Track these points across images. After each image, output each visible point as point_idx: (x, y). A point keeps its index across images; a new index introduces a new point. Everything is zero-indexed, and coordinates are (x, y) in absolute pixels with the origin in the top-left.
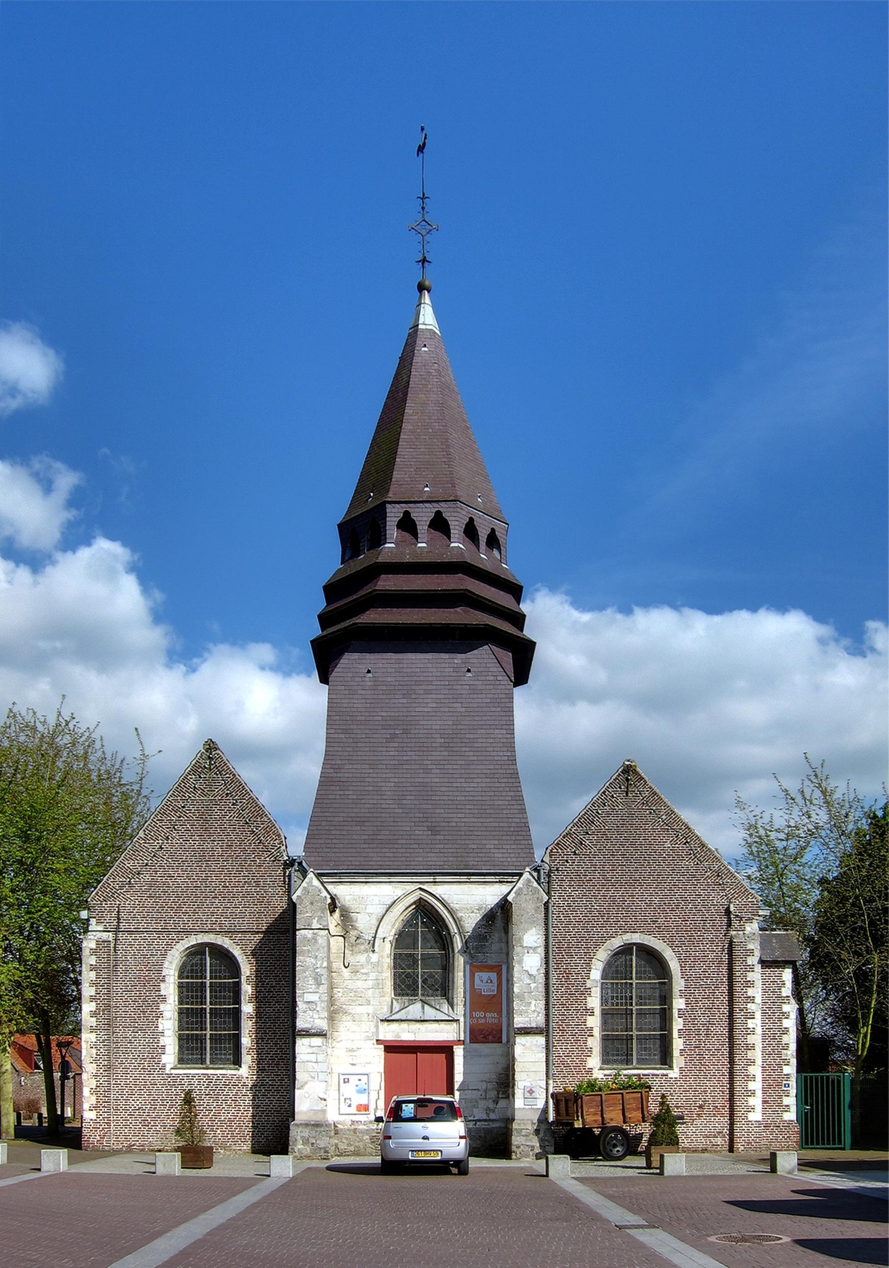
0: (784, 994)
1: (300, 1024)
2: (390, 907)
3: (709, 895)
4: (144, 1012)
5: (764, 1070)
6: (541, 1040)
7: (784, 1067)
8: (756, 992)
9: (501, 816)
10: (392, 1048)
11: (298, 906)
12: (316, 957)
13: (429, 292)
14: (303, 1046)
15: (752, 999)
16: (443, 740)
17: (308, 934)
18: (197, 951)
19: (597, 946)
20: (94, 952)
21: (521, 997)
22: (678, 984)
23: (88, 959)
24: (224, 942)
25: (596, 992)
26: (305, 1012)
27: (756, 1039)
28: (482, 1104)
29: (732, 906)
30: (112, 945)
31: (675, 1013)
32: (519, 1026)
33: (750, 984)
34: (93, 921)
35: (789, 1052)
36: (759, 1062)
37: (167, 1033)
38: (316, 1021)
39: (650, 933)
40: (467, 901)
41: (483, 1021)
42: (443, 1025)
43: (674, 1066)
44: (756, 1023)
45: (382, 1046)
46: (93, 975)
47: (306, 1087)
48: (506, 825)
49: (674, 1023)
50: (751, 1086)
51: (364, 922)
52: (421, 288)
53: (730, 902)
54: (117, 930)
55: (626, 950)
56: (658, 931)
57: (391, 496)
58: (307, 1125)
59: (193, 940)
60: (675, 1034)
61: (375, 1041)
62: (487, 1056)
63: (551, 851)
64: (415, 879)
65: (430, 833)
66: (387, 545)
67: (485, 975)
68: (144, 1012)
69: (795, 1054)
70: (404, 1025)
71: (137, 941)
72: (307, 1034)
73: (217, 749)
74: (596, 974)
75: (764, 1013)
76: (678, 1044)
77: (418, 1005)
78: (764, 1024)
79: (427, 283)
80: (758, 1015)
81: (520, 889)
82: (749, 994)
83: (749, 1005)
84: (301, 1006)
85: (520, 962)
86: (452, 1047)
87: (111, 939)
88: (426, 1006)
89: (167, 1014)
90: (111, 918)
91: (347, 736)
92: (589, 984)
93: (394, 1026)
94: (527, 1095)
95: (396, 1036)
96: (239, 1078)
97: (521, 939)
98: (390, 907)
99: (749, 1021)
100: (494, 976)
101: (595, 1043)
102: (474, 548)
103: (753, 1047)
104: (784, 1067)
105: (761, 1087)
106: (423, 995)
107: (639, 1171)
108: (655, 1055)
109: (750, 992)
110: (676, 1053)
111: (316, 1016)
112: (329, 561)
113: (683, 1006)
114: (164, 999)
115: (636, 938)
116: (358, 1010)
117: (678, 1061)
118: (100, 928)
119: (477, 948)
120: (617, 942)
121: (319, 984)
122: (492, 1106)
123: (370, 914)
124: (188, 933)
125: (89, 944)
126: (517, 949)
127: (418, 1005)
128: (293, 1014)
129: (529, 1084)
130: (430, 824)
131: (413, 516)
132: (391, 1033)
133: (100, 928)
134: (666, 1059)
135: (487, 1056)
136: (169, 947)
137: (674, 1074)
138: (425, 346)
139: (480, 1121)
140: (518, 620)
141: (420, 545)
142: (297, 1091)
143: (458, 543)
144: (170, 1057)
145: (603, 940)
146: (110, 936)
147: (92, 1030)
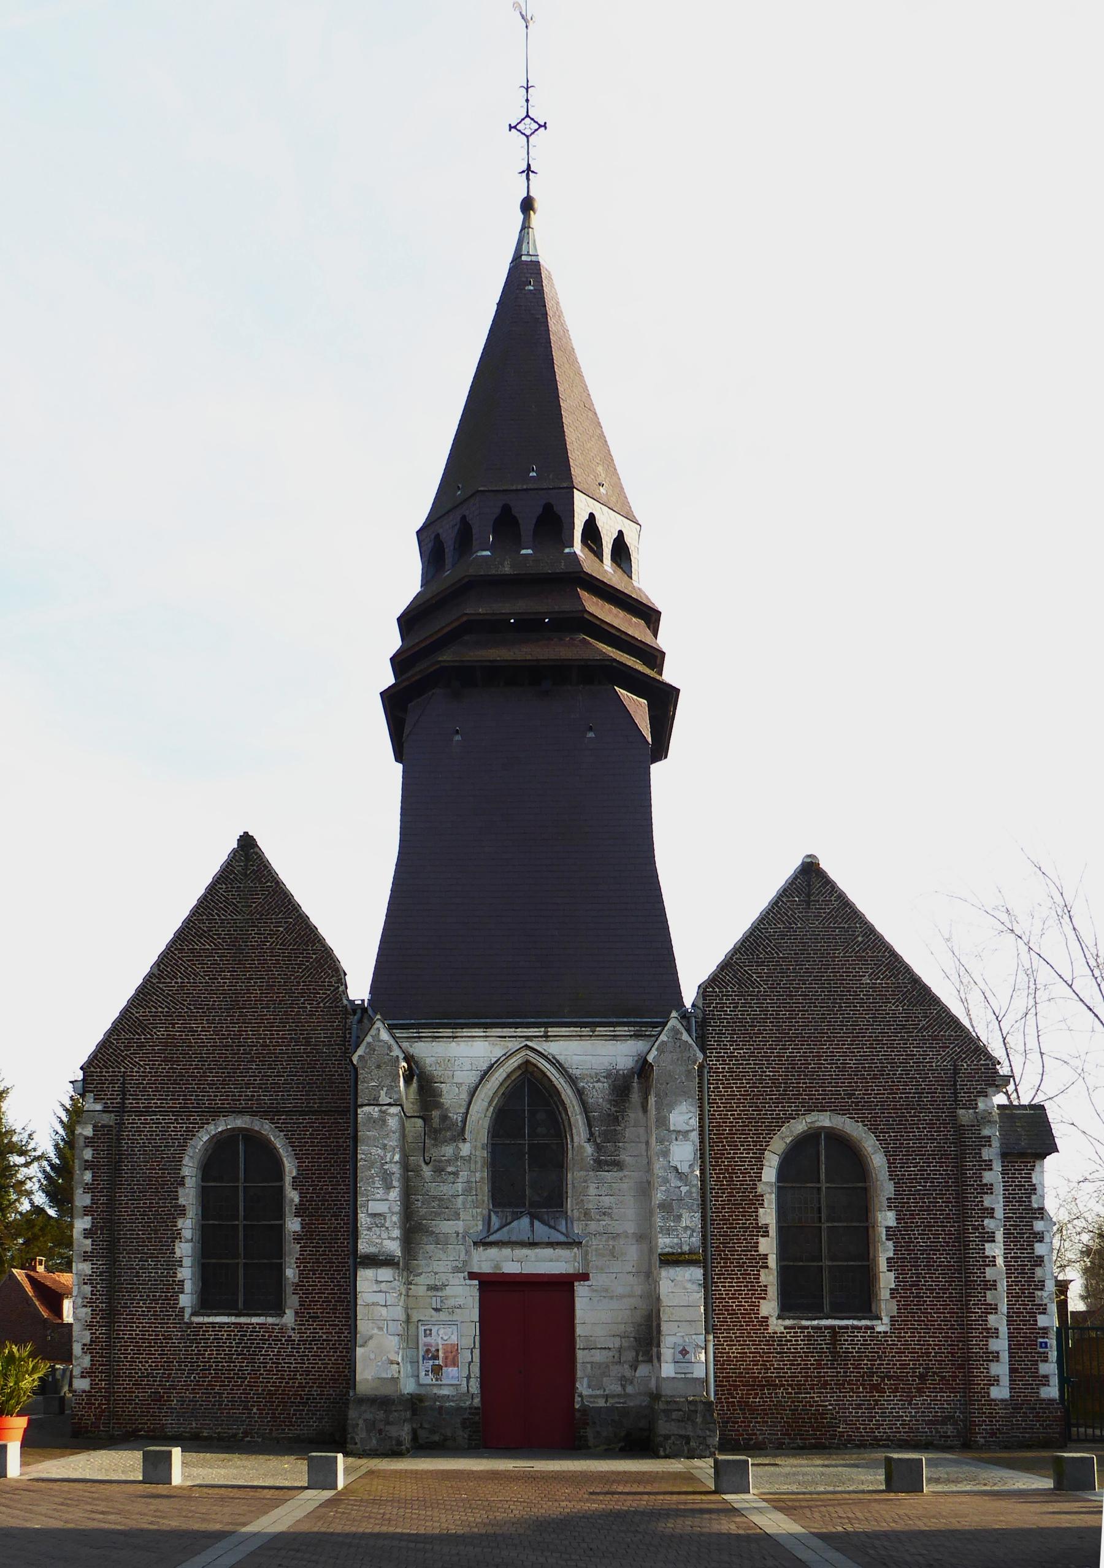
1: (363, 1247)
2: (486, 1073)
4: (156, 1231)
5: (1010, 1322)
6: (697, 1273)
8: (996, 1202)
10: (492, 1286)
17: (374, 1111)
18: (222, 1145)
22: (886, 1188)
24: (265, 1128)
28: (615, 1370)
44: (996, 1250)
45: (477, 1282)
47: (371, 1343)
50: (995, 1345)
51: (452, 1096)
54: (121, 1110)
59: (221, 1125)
62: (621, 1297)
68: (156, 1231)
70: (507, 1251)
74: (769, 1174)
75: (1007, 1234)
76: (886, 1280)
77: (525, 1221)
78: (1007, 1249)
80: (999, 1236)
82: (986, 1204)
88: (536, 1223)
89: (187, 1234)
93: (493, 1252)
96: (283, 1329)
99: (987, 1245)
101: (769, 1278)
103: (993, 1286)
104: (1039, 1317)
109: (988, 1201)
113: (892, 1223)
114: (182, 1211)
115: (825, 1120)
117: (887, 1307)
120: (799, 1126)
121: (389, 1187)
122: (628, 1373)
124: (216, 1113)
127: (525, 1221)
128: (354, 1234)
129: (680, 1341)
132: (487, 1261)
134: (863, 1303)
139: (613, 1396)
140: (655, 658)
141: (523, 552)
144: (186, 1300)
145: (780, 1122)
147: (86, 1257)
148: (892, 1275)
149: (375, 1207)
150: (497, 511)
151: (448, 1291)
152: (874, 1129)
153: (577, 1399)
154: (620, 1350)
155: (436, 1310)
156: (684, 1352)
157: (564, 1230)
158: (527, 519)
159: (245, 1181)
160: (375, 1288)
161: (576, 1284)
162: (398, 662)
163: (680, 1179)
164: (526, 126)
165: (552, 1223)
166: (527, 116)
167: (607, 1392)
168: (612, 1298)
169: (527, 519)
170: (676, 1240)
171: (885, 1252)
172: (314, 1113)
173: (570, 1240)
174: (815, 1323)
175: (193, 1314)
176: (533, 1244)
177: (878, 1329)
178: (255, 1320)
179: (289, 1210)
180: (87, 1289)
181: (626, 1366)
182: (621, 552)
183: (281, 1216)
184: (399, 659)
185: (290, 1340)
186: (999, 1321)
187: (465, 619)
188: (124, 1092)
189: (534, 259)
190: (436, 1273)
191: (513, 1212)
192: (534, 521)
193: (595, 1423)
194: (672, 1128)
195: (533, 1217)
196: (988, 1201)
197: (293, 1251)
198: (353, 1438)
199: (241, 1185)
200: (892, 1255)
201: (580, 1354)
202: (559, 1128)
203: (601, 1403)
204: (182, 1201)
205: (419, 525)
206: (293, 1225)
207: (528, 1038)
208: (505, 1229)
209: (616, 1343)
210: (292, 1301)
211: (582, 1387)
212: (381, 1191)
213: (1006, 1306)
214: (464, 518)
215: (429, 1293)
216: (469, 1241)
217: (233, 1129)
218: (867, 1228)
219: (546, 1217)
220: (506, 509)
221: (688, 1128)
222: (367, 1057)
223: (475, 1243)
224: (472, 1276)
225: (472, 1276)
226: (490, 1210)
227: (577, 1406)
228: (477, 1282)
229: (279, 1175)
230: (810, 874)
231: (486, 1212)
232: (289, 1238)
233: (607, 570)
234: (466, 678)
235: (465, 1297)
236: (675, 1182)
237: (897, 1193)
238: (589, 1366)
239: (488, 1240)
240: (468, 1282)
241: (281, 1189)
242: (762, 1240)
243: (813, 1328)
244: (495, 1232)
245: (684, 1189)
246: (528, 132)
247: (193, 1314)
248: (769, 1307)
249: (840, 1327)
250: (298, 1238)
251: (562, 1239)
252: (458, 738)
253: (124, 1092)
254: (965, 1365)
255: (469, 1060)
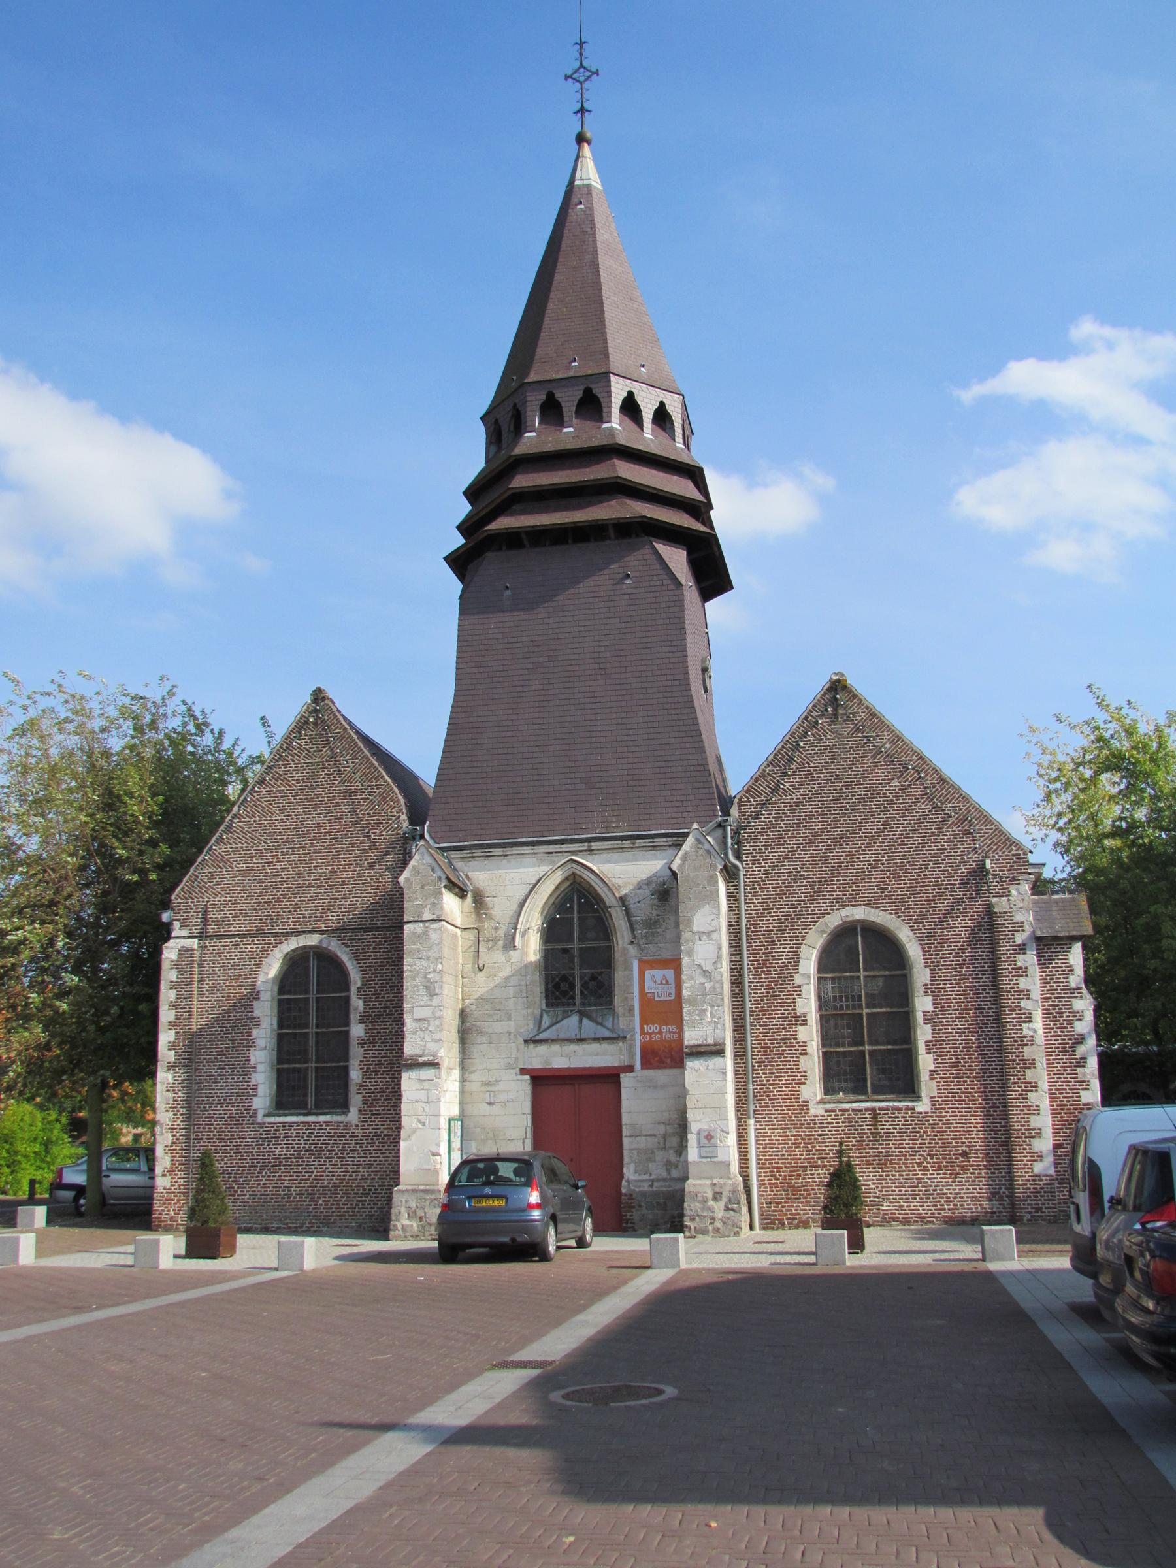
0: (1073, 985)
1: (410, 1048)
2: (535, 886)
3: (955, 849)
4: (233, 1041)
5: (1052, 1097)
7: (1082, 1093)
9: (673, 758)
10: (541, 1080)
11: (406, 892)
12: (428, 959)
13: (589, 144)
14: (409, 1081)
15: (1026, 994)
16: (597, 666)
19: (806, 927)
20: (176, 964)
21: (693, 1003)
22: (921, 976)
23: (169, 975)
25: (810, 991)
26: (415, 1033)
27: (1037, 1053)
28: (660, 1156)
29: (988, 862)
30: (197, 955)
31: (919, 1017)
32: (693, 1042)
33: (1021, 972)
34: (177, 924)
35: (1088, 1071)
36: (1044, 1085)
37: (260, 1068)
38: (429, 1045)
39: (876, 905)
40: (623, 872)
41: (657, 1037)
42: (605, 1046)
43: (923, 1094)
45: (528, 1077)
46: (172, 994)
47: (414, 1138)
48: (680, 769)
49: (919, 1032)
50: (1035, 1122)
52: (581, 139)
53: (987, 857)
55: (847, 931)
56: (889, 903)
57: (532, 377)
58: (414, 1191)
59: (293, 944)
60: (921, 1047)
61: (518, 1071)
62: (664, 1087)
63: (740, 800)
64: (565, 847)
65: (583, 786)
66: (527, 435)
67: (658, 973)
68: (233, 1041)
69: (1096, 1073)
70: (556, 1048)
71: (226, 948)
72: (416, 1065)
73: (324, 699)
75: (1046, 1013)
76: (926, 1062)
77: (575, 1018)
78: (1047, 1029)
79: (588, 135)
80: (1038, 1017)
81: (687, 853)
82: (1022, 986)
83: (1023, 1003)
84: (409, 1025)
85: (690, 953)
86: (618, 1076)
87: (196, 947)
88: (585, 1020)
89: (261, 1043)
90: (195, 919)
91: (481, 670)
92: (798, 980)
93: (543, 1048)
94: (704, 1141)
95: (547, 1062)
96: (347, 1126)
97: (689, 922)
98: (535, 886)
99: (1025, 1025)
100: (670, 973)
101: (812, 1063)
102: (633, 426)
103: (1033, 1065)
104: (1082, 1093)
105: (1050, 1123)
106: (583, 1004)
107: (937, 1256)
108: (898, 1079)
109: (1023, 983)
110: (924, 1075)
111: (428, 1038)
112: (471, 458)
113: (930, 1008)
114: (257, 1022)
115: (859, 913)
116: (498, 1027)
117: (928, 1087)
118: (185, 933)
119: (647, 936)
120: (834, 920)
123: (509, 898)
125: (170, 953)
126: (686, 936)
127: (575, 1018)
128: (399, 1037)
129: (705, 1127)
130: (583, 775)
131: (638, 398)
133: (185, 933)
134: (908, 1087)
135: (664, 1087)
136: (265, 953)
137: (923, 1106)
138: (581, 203)
139: (658, 1180)
141: (566, 430)
142: (403, 1144)
143: (615, 422)
144: (261, 1102)
145: (815, 917)
146: (194, 943)
147: (170, 1067)
148: (931, 1057)
149: (419, 1013)
150: (543, 397)
151: (501, 1086)
152: (907, 918)
153: (624, 1183)
154: (665, 1137)
155: (490, 1104)
156: (709, 1137)
157: (610, 1025)
158: (569, 399)
159: (318, 992)
160: (418, 1086)
161: (622, 1075)
162: (466, 528)
163: (704, 976)
164: (582, 75)
165: (600, 1019)
166: (581, 66)
167: (653, 1177)
168: (655, 1087)
169: (569, 399)
170: (701, 1033)
171: (923, 1034)
172: (377, 929)
173: (615, 1035)
174: (855, 1105)
175: (265, 1115)
176: (581, 1040)
177: (918, 1109)
178: (322, 1118)
179: (354, 1017)
180: (170, 1095)
181: (671, 1152)
182: (662, 417)
183: (347, 1023)
184: (465, 526)
185: (353, 1136)
186: (1041, 1098)
187: (510, 492)
188: (205, 919)
189: (586, 182)
190: (490, 1070)
191: (564, 1012)
192: (575, 403)
193: (640, 1206)
194: (696, 929)
195: (582, 1014)
196: (1023, 983)
197: (356, 1054)
198: (395, 1226)
199: (312, 996)
200: (930, 1038)
201: (626, 1142)
202: (604, 931)
203: (645, 1187)
204: (257, 1013)
205: (484, 411)
206: (357, 1030)
207: (574, 853)
208: (554, 1028)
209: (662, 1129)
210: (356, 1100)
211: (629, 1172)
212: (425, 998)
213: (1046, 1084)
214: (515, 405)
215: (484, 1089)
216: (521, 1041)
217: (305, 947)
218: (908, 1013)
219: (594, 1015)
220: (551, 396)
221: (711, 929)
222: (412, 879)
223: (526, 1042)
224: (523, 1071)
225: (523, 1071)
226: (542, 1010)
227: (624, 1191)
228: (528, 1077)
229: (345, 984)
230: (837, 687)
231: (538, 1012)
232: (354, 1043)
233: (648, 437)
234: (514, 540)
235: (520, 1092)
236: (700, 979)
237: (933, 979)
238: (635, 1152)
239: (537, 1038)
240: (520, 1077)
241: (347, 1000)
242: (800, 1028)
243: (854, 1110)
244: (546, 1030)
245: (708, 985)
246: (582, 79)
247: (265, 1115)
248: (812, 1090)
249: (881, 1109)
250: (362, 1043)
251: (607, 1034)
252: (508, 592)
253: (205, 919)
254: (1001, 1145)
255: (522, 885)
